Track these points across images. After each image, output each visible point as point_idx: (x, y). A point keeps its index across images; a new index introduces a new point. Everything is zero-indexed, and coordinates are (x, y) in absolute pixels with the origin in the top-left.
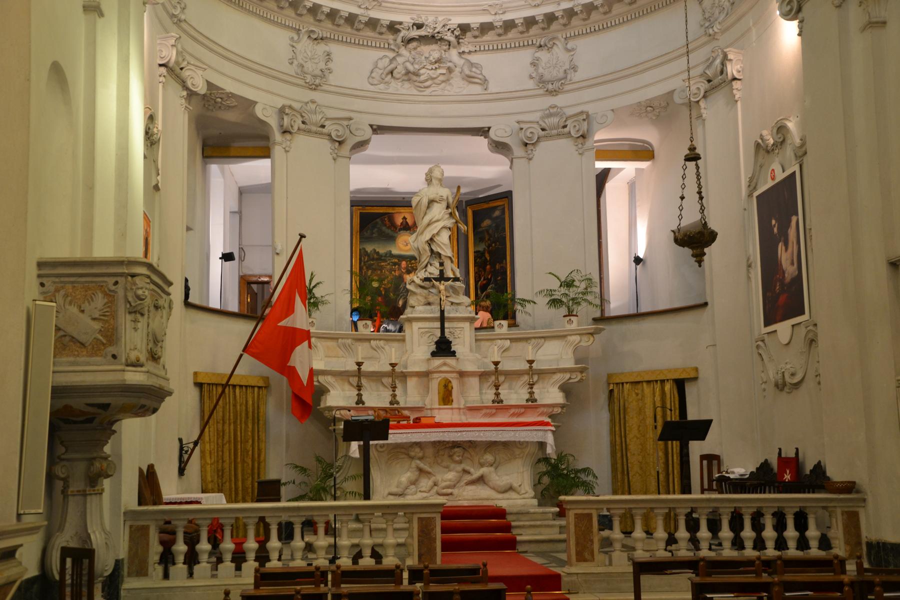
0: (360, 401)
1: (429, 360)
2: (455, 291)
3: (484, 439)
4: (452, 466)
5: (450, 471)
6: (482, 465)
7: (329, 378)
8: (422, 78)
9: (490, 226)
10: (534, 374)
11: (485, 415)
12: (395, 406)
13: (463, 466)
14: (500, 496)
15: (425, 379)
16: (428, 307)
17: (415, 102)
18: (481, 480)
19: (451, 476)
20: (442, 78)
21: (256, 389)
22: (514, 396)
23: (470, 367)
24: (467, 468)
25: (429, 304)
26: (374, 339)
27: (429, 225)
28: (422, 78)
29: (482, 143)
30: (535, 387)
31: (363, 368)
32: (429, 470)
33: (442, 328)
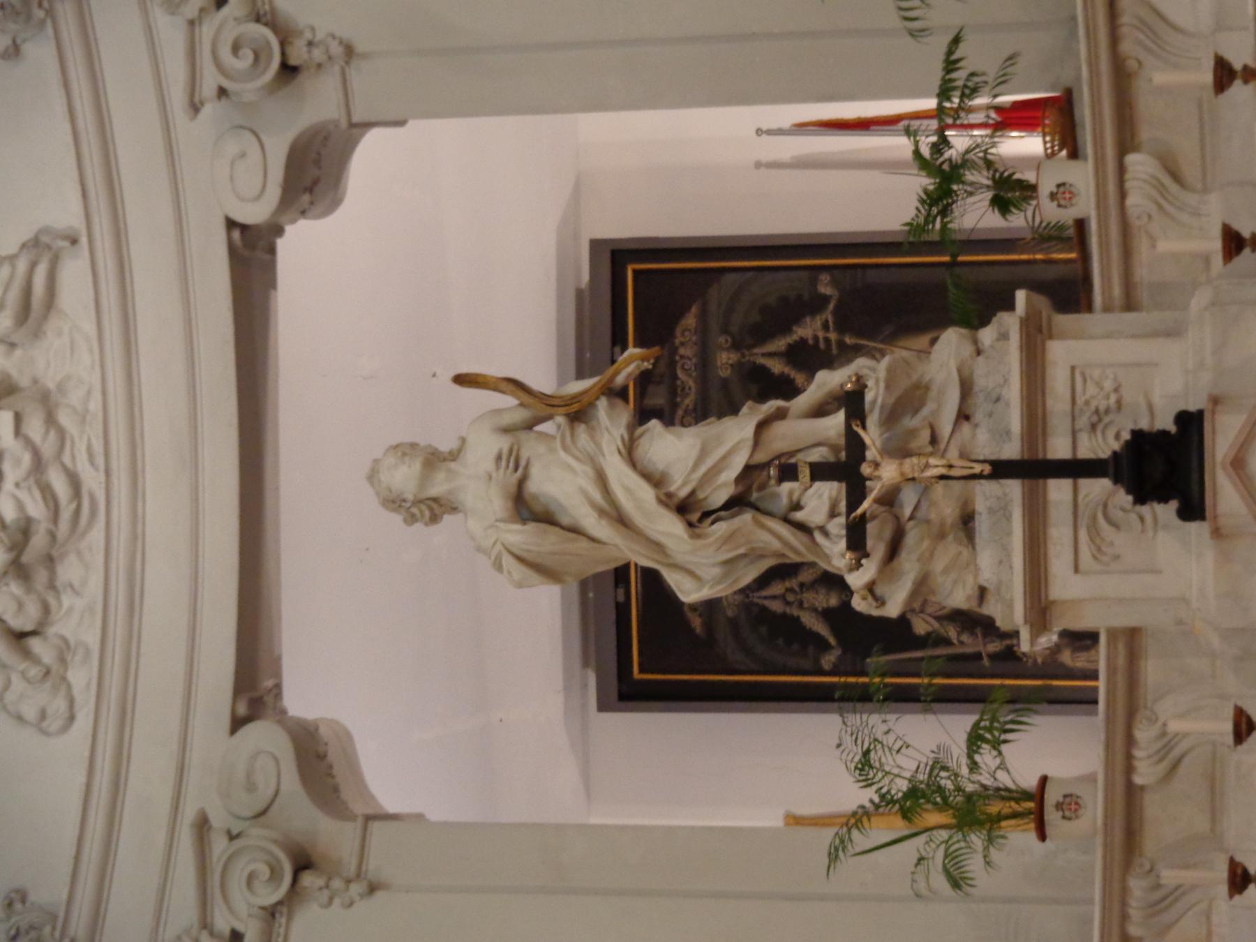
1: (1217, 533)
2: (910, 399)
8: (36, 509)
16: (982, 525)
17: (137, 536)
20: (35, 428)
25: (967, 520)
26: (1129, 769)
27: (621, 520)
28: (36, 509)
29: (302, 246)
33: (1076, 469)
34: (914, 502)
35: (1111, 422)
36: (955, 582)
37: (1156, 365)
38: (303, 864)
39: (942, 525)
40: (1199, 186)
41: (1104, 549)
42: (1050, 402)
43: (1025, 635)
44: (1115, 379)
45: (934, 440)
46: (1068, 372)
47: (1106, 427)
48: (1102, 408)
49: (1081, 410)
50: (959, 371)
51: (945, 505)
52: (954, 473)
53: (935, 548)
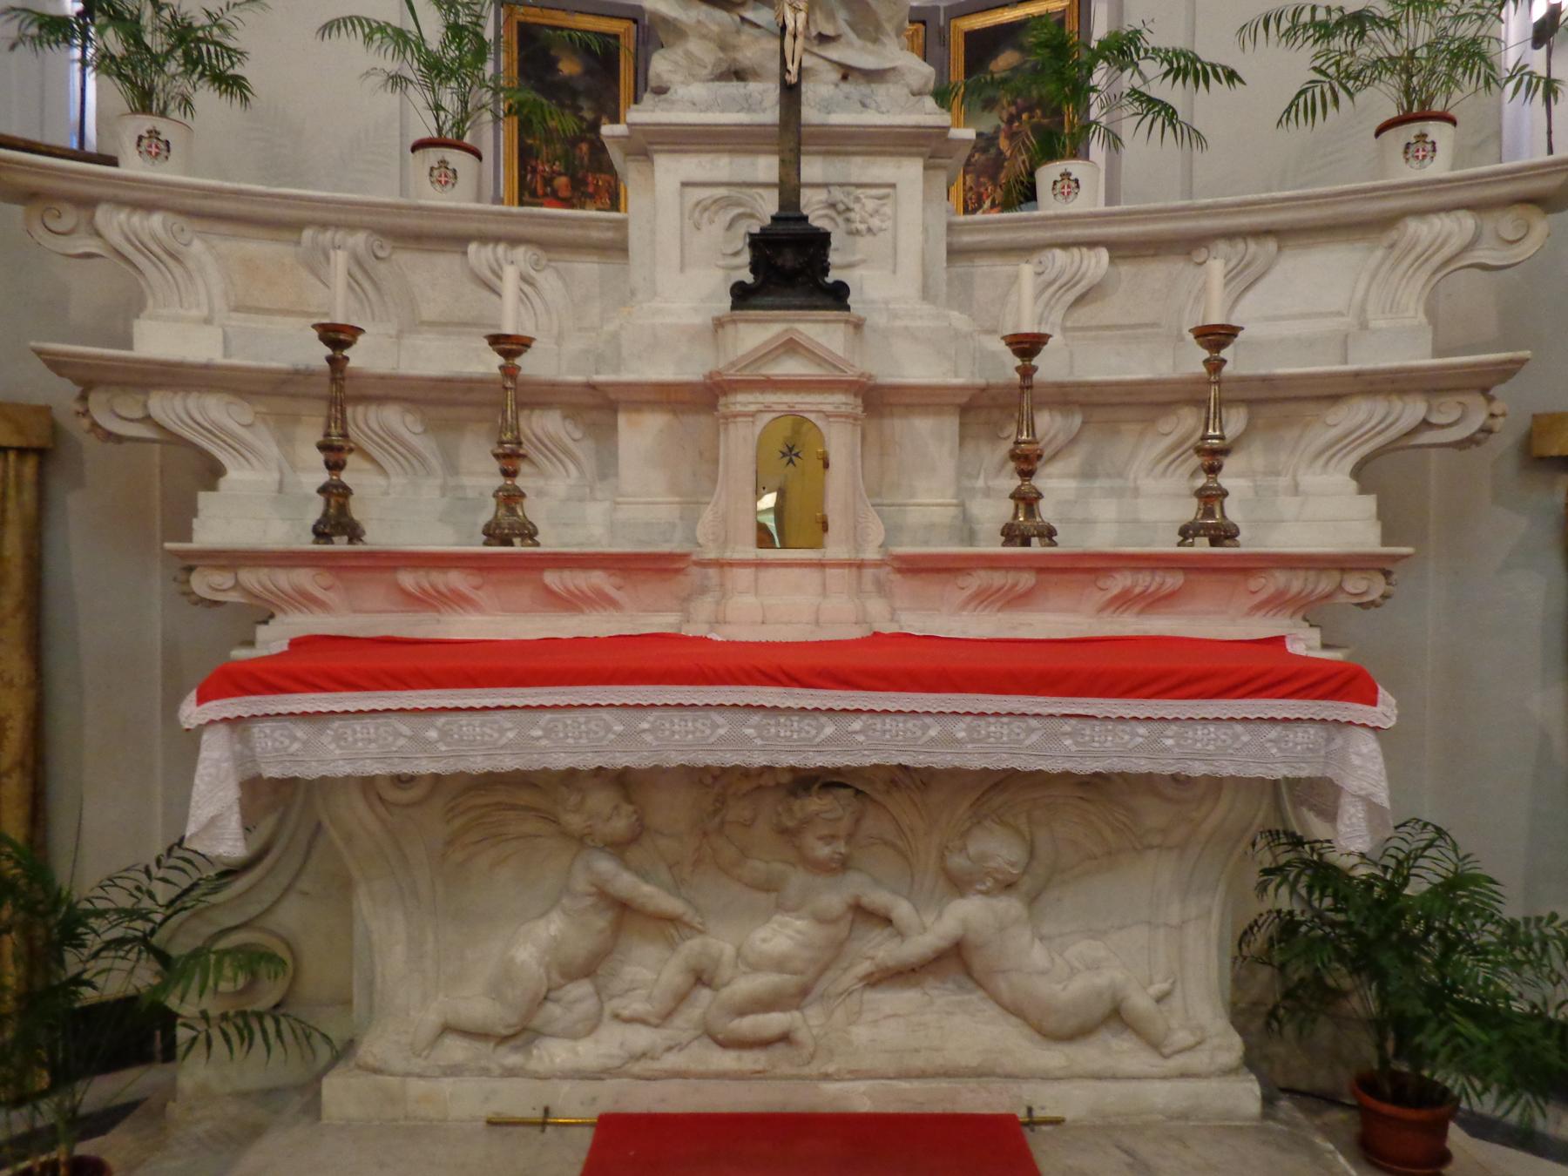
0: (337, 520)
1: (719, 324)
3: (976, 763)
4: (798, 879)
5: (780, 908)
6: (959, 885)
7: (215, 409)
9: (1015, 69)
10: (1226, 403)
11: (983, 598)
12: (518, 548)
13: (855, 886)
14: (1055, 1057)
15: (704, 421)
16: (733, 88)
18: (955, 961)
19: (781, 936)
21: (12, 456)
22: (1106, 510)
23: (916, 368)
24: (878, 898)
25: (738, 74)
26: (484, 239)
30: (1230, 464)
31: (358, 357)
32: (670, 904)
34: (759, 22)
35: (836, 224)
36: (676, 63)
37: (894, 272)
38: (817, 623)
39: (734, 47)
40: (1069, 324)
41: (706, 215)
42: (858, 160)
43: (620, 129)
44: (881, 230)
45: (823, 39)
46: (892, 181)
47: (832, 219)
48: (852, 215)
49: (849, 194)
50: (894, 69)
51: (756, 50)
52: (788, 39)
53: (710, 39)
